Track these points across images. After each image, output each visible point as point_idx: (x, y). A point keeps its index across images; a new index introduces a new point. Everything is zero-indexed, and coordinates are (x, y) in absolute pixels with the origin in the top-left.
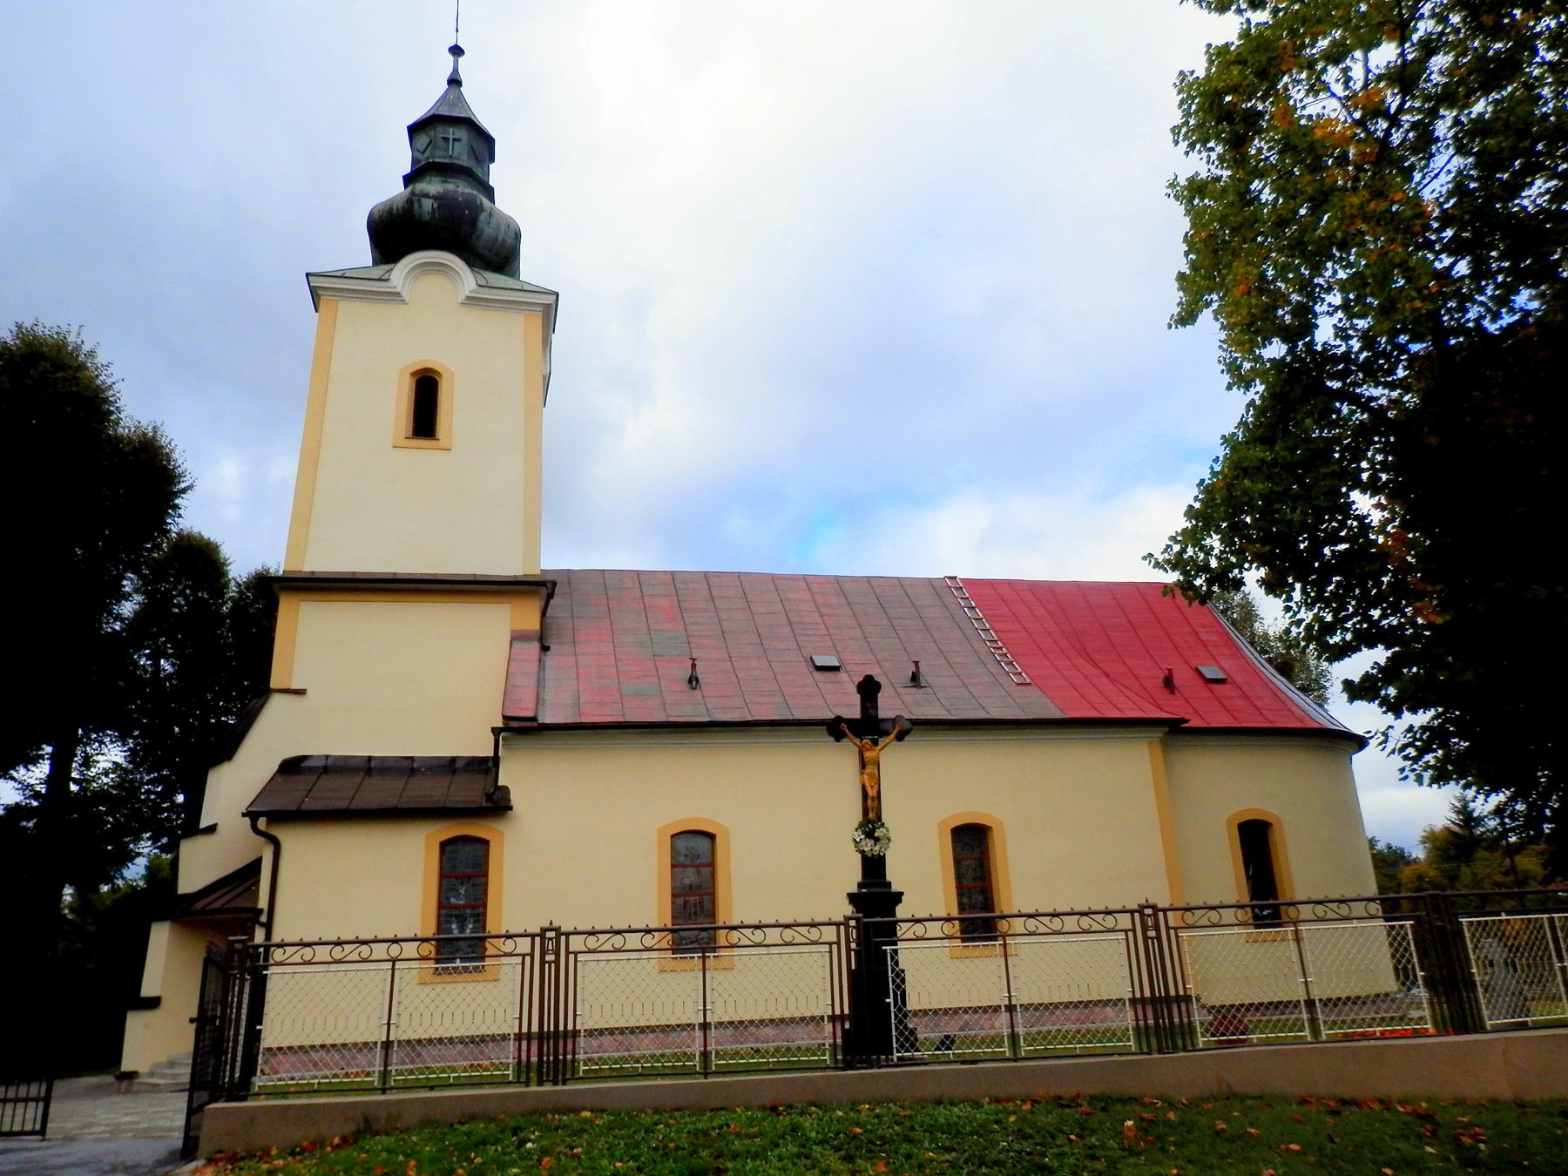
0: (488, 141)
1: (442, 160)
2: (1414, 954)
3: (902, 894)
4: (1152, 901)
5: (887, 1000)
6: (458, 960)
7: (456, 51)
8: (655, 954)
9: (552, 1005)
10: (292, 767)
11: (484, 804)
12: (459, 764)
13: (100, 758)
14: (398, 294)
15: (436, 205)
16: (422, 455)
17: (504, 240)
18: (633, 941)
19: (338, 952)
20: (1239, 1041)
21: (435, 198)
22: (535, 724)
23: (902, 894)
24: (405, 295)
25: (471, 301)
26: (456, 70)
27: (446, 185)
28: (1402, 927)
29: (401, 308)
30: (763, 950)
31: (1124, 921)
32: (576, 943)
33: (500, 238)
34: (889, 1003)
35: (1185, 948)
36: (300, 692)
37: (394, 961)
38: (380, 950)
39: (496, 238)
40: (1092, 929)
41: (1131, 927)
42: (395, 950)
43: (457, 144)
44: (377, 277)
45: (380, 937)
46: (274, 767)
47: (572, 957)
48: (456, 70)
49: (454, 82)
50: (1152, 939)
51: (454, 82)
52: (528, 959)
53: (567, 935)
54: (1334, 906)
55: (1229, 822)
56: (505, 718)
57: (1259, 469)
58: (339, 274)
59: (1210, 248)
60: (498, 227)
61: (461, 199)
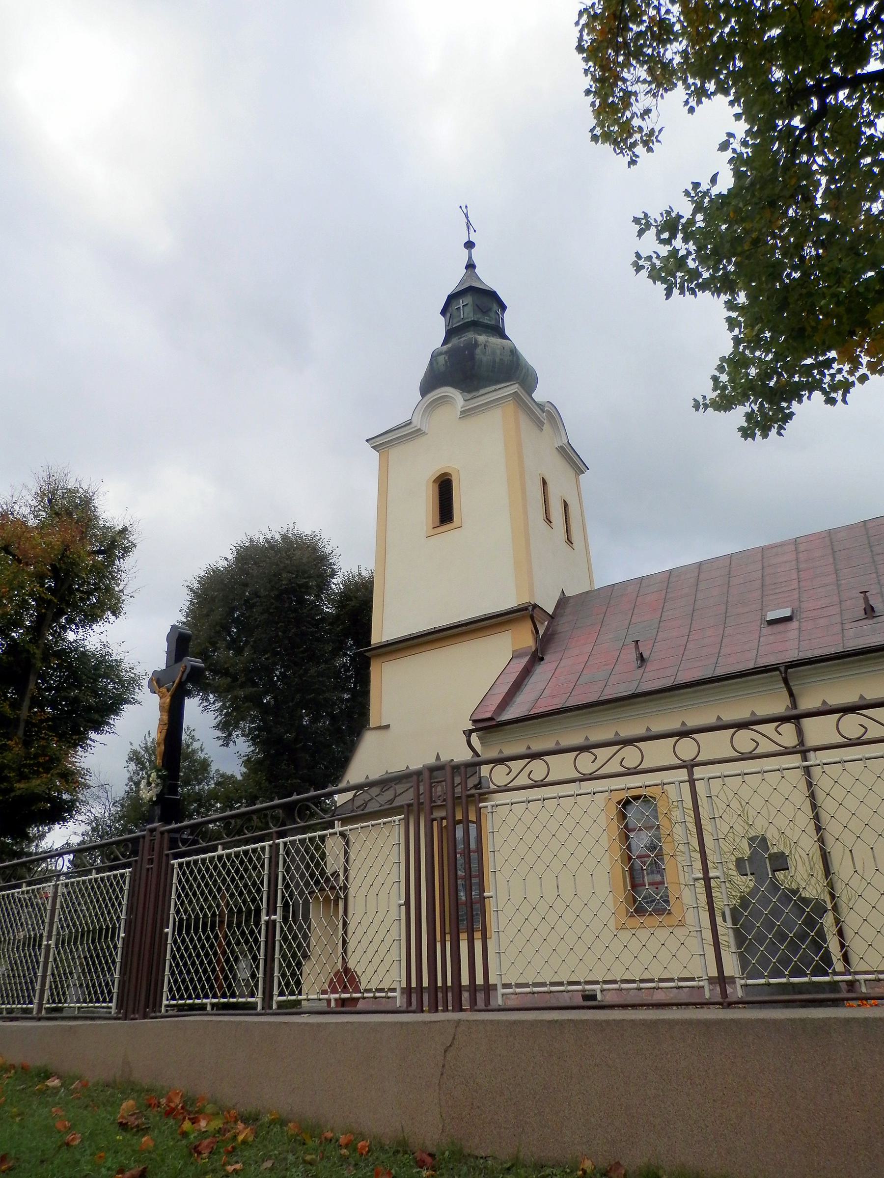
0: (492, 295)
1: (458, 324)
2: (196, 821)
5: (166, 930)
6: (24, 885)
7: (469, 245)
14: (419, 430)
16: (449, 536)
17: (501, 360)
20: (192, 1007)
22: (494, 723)
24: (423, 428)
25: (466, 414)
26: (470, 258)
29: (423, 439)
33: (497, 360)
34: (167, 934)
36: (387, 727)
39: (494, 361)
40: (868, 736)
43: (465, 308)
48: (470, 258)
49: (470, 266)
51: (470, 266)
56: (475, 722)
57: (604, 65)
60: (494, 353)
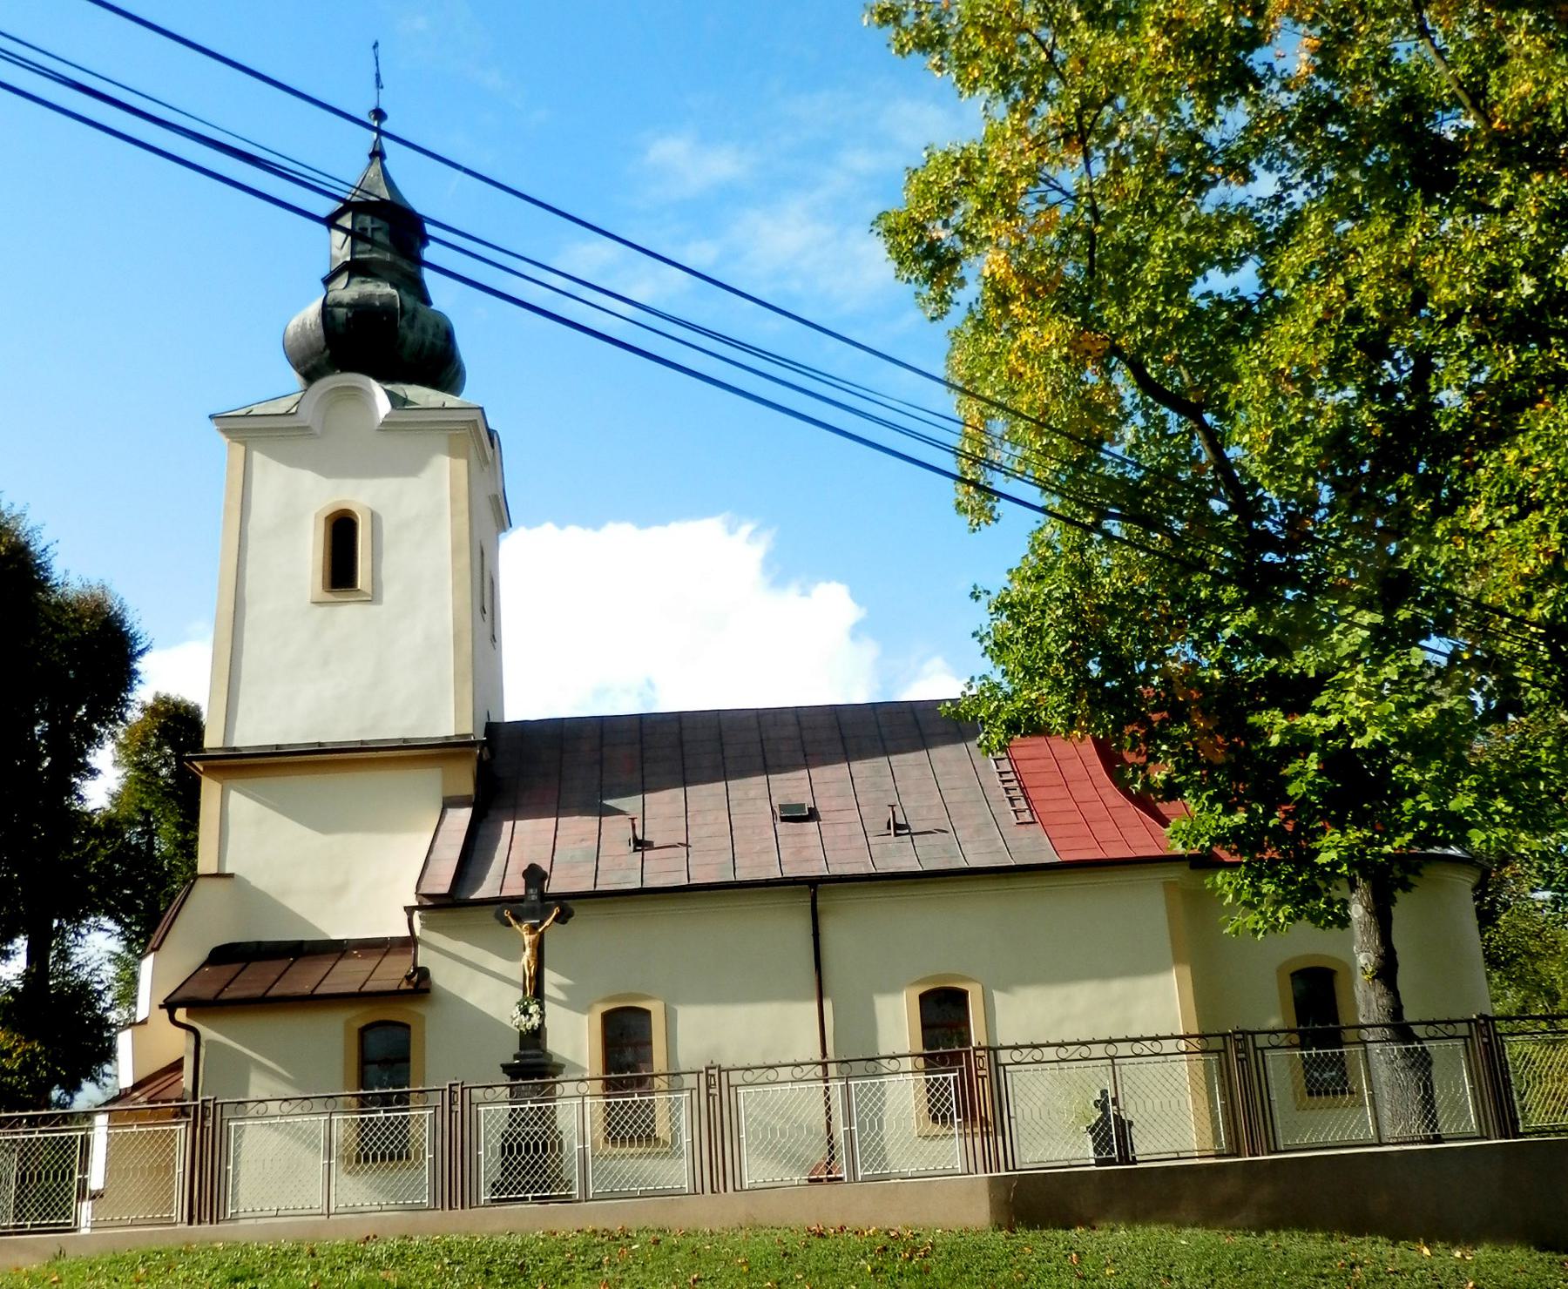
3: (502, 1066)
4: (716, 1063)
8: (1185, 1056)
9: (1255, 1076)
10: (222, 955)
11: (404, 986)
12: (306, 948)
13: (77, 950)
15: (350, 315)
18: (1169, 1046)
19: (1063, 1053)
21: (349, 306)
23: (502, 1066)
27: (364, 286)
28: (945, 1079)
30: (1162, 1058)
31: (1463, 1029)
32: (736, 1077)
35: (1270, 1065)
37: (1112, 1058)
38: (1098, 1050)
41: (1222, 1048)
42: (1111, 1050)
44: (283, 411)
45: (783, 1062)
46: (203, 956)
47: (732, 1089)
50: (983, 1077)
52: (695, 1093)
53: (728, 1071)
54: (1441, 1026)
55: (1280, 970)
58: (243, 412)
59: (1446, 403)
61: (377, 303)
